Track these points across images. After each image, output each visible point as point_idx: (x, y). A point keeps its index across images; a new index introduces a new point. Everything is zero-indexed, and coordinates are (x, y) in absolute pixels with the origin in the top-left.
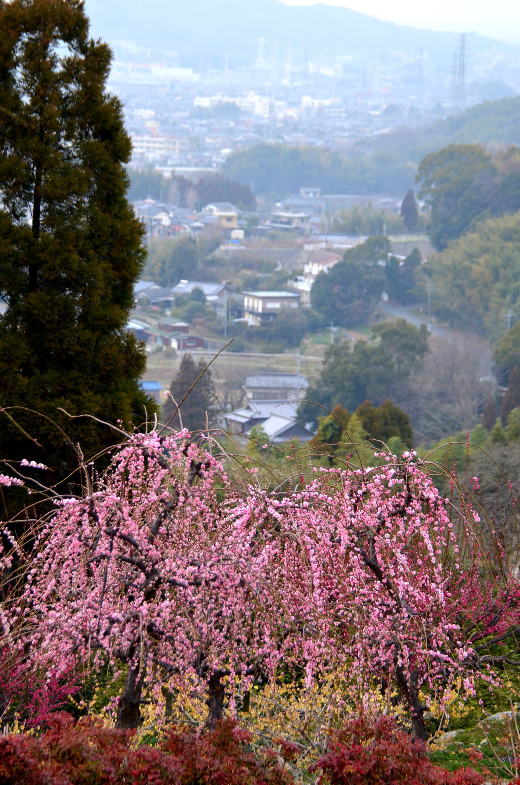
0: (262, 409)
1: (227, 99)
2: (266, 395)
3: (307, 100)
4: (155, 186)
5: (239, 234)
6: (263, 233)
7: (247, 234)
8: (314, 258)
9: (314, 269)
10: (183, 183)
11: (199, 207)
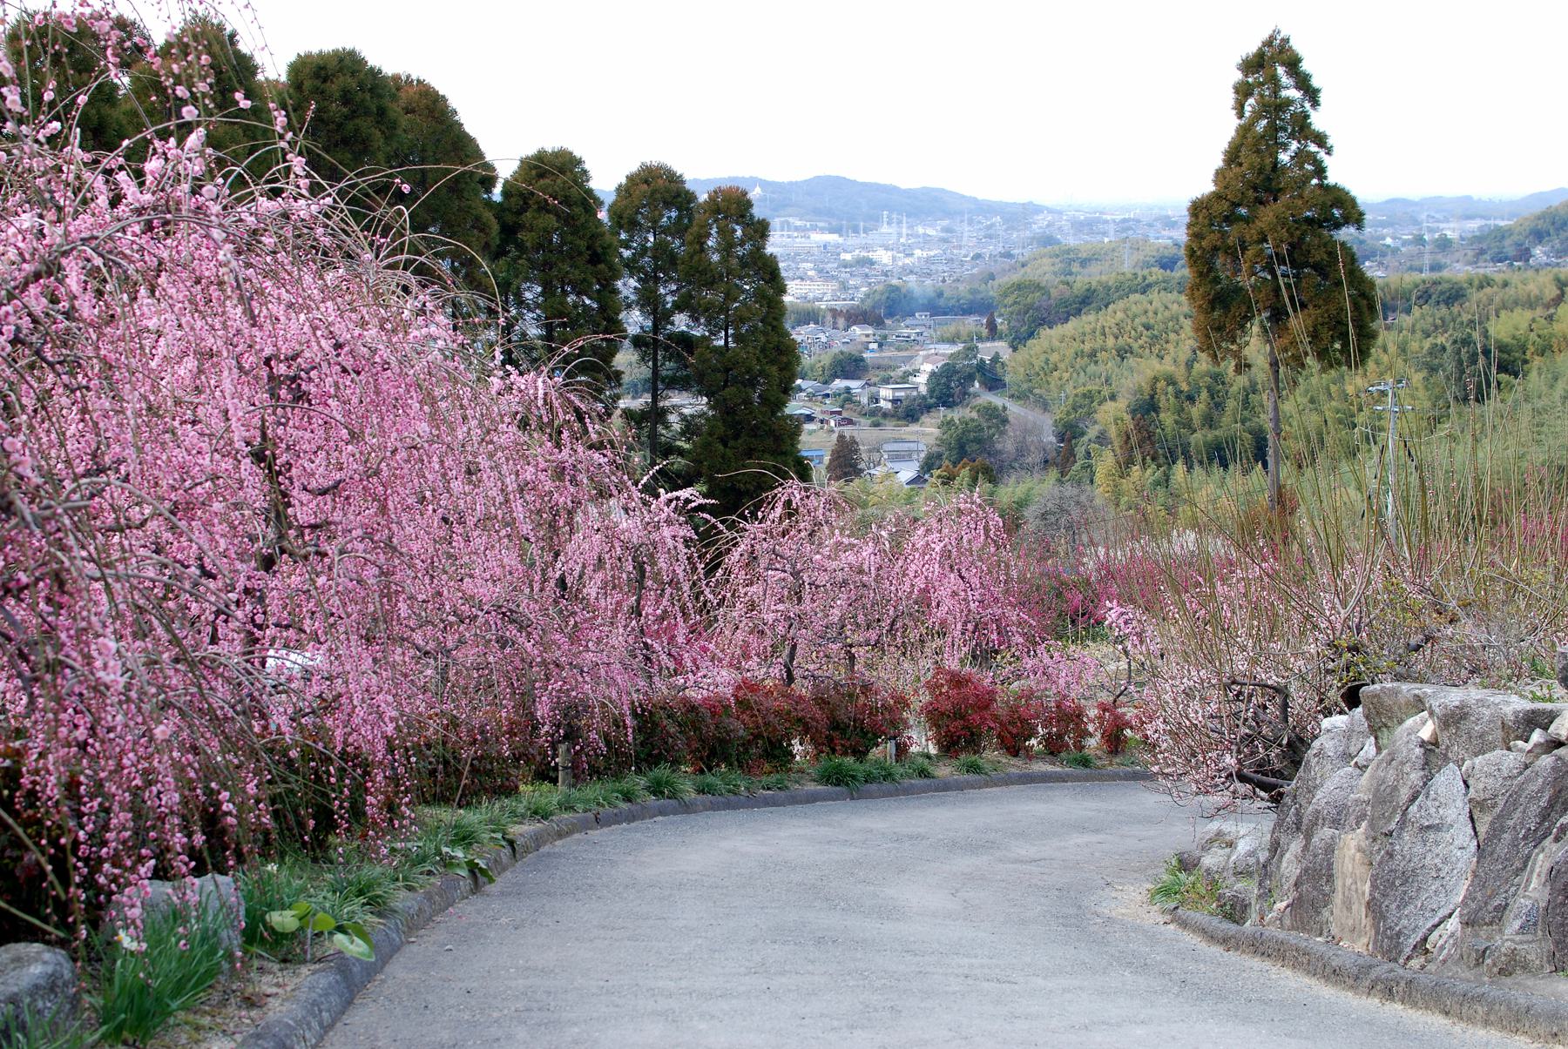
0: (896, 466)
1: (864, 254)
2: (897, 457)
3: (918, 253)
4: (809, 316)
5: (874, 346)
6: (891, 344)
7: (880, 345)
8: (926, 359)
9: (928, 368)
10: (835, 313)
11: (846, 330)
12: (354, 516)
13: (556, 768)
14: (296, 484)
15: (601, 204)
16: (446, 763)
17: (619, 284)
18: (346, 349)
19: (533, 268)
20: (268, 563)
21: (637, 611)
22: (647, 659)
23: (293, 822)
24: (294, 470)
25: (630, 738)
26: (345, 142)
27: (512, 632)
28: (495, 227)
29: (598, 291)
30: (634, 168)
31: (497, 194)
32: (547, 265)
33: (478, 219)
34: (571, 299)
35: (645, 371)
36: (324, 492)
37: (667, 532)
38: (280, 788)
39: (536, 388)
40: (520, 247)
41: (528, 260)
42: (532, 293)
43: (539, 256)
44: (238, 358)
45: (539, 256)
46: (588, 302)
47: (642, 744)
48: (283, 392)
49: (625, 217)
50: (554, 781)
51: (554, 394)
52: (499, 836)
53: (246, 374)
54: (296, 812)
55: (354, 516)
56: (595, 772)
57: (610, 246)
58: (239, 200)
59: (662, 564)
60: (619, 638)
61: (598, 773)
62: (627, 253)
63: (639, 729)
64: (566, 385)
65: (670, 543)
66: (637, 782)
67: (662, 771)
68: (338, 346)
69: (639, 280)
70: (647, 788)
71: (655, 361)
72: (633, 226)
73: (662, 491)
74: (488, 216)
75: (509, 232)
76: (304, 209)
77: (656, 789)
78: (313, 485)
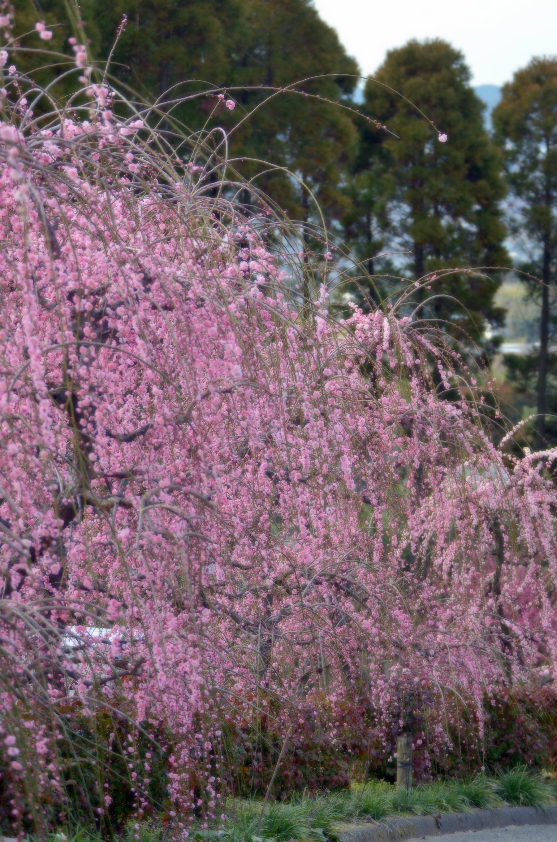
12: (165, 467)
13: (393, 766)
14: (100, 428)
15: (483, 107)
16: (265, 751)
17: (503, 205)
18: (156, 283)
19: (402, 184)
20: (68, 514)
21: (495, 589)
22: (506, 644)
23: (87, 800)
24: (97, 414)
25: (481, 734)
26: (179, 32)
27: (348, 605)
28: (354, 136)
29: (478, 213)
30: (522, 62)
31: (358, 97)
32: (416, 182)
33: (334, 125)
34: (445, 221)
35: (533, 311)
36: (130, 438)
37: (531, 497)
38: (75, 762)
39: (381, 330)
40: (386, 158)
41: (396, 174)
42: (399, 213)
43: (408, 170)
44: (40, 293)
45: (408, 170)
46: (465, 225)
47: (496, 742)
48: (87, 330)
49: (512, 123)
50: (391, 779)
51: (400, 335)
52: (319, 831)
53: (49, 309)
54: (91, 789)
55: (165, 467)
56: (439, 771)
57: (493, 158)
58: (40, 125)
59: (527, 533)
60: (474, 616)
61: (443, 772)
62: (515, 168)
63: (491, 724)
64: (414, 326)
65: (534, 509)
66: (488, 785)
67: (518, 774)
68: (147, 281)
69: (529, 199)
70: (499, 793)
71: (545, 296)
72: (521, 133)
73: (527, 450)
74: (346, 123)
75: (372, 139)
76: (110, 131)
77: (510, 794)
78: (120, 431)
